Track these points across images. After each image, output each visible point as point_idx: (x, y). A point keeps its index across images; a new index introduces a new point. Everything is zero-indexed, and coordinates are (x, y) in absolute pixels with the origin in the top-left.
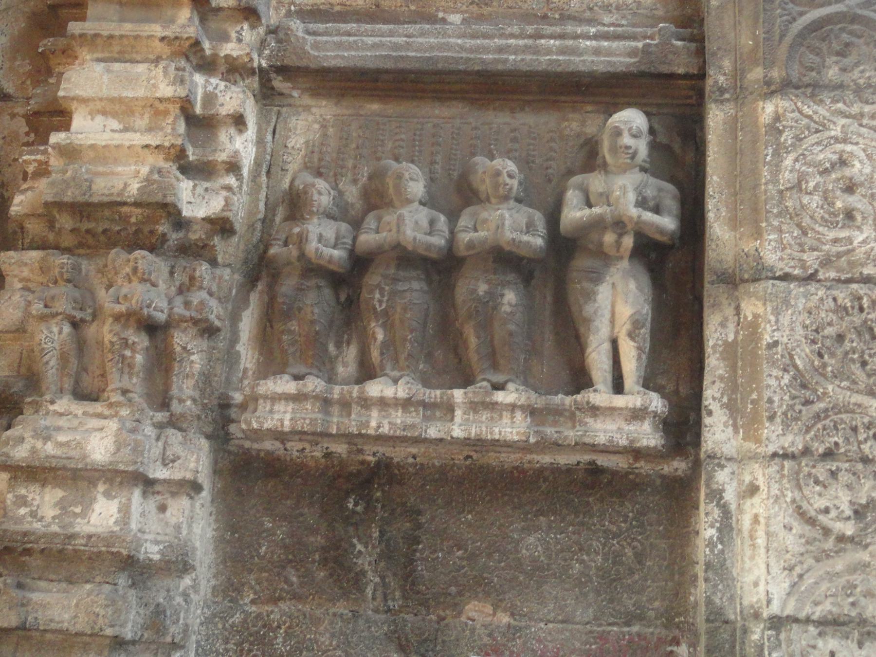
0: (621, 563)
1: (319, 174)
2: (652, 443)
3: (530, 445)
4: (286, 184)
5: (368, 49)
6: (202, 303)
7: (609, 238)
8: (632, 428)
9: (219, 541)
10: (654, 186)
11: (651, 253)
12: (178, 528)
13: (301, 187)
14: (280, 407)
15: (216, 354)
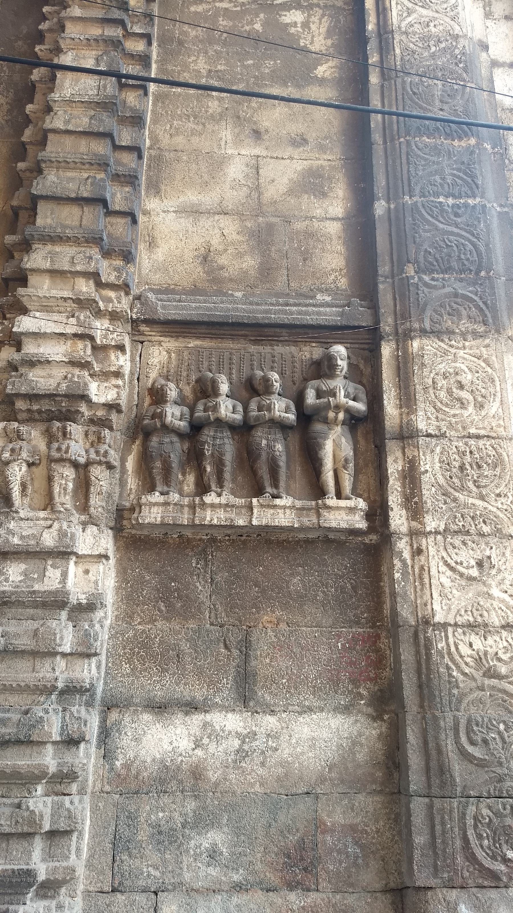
0: (345, 593)
1: (169, 380)
2: (361, 526)
3: (295, 528)
4: (149, 385)
5: (193, 310)
6: (106, 452)
7: (331, 415)
8: (349, 518)
9: (118, 589)
10: (352, 387)
11: (353, 422)
12: (96, 583)
13: (159, 387)
14: (155, 509)
15: (114, 481)
